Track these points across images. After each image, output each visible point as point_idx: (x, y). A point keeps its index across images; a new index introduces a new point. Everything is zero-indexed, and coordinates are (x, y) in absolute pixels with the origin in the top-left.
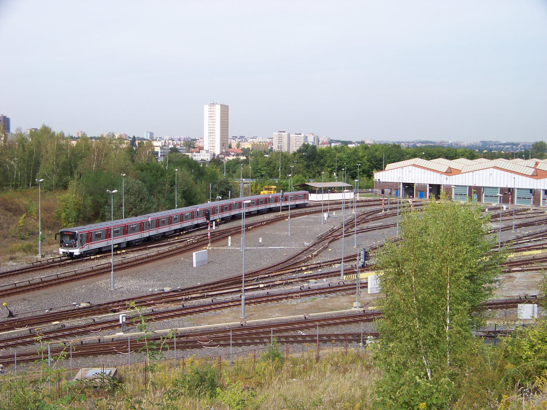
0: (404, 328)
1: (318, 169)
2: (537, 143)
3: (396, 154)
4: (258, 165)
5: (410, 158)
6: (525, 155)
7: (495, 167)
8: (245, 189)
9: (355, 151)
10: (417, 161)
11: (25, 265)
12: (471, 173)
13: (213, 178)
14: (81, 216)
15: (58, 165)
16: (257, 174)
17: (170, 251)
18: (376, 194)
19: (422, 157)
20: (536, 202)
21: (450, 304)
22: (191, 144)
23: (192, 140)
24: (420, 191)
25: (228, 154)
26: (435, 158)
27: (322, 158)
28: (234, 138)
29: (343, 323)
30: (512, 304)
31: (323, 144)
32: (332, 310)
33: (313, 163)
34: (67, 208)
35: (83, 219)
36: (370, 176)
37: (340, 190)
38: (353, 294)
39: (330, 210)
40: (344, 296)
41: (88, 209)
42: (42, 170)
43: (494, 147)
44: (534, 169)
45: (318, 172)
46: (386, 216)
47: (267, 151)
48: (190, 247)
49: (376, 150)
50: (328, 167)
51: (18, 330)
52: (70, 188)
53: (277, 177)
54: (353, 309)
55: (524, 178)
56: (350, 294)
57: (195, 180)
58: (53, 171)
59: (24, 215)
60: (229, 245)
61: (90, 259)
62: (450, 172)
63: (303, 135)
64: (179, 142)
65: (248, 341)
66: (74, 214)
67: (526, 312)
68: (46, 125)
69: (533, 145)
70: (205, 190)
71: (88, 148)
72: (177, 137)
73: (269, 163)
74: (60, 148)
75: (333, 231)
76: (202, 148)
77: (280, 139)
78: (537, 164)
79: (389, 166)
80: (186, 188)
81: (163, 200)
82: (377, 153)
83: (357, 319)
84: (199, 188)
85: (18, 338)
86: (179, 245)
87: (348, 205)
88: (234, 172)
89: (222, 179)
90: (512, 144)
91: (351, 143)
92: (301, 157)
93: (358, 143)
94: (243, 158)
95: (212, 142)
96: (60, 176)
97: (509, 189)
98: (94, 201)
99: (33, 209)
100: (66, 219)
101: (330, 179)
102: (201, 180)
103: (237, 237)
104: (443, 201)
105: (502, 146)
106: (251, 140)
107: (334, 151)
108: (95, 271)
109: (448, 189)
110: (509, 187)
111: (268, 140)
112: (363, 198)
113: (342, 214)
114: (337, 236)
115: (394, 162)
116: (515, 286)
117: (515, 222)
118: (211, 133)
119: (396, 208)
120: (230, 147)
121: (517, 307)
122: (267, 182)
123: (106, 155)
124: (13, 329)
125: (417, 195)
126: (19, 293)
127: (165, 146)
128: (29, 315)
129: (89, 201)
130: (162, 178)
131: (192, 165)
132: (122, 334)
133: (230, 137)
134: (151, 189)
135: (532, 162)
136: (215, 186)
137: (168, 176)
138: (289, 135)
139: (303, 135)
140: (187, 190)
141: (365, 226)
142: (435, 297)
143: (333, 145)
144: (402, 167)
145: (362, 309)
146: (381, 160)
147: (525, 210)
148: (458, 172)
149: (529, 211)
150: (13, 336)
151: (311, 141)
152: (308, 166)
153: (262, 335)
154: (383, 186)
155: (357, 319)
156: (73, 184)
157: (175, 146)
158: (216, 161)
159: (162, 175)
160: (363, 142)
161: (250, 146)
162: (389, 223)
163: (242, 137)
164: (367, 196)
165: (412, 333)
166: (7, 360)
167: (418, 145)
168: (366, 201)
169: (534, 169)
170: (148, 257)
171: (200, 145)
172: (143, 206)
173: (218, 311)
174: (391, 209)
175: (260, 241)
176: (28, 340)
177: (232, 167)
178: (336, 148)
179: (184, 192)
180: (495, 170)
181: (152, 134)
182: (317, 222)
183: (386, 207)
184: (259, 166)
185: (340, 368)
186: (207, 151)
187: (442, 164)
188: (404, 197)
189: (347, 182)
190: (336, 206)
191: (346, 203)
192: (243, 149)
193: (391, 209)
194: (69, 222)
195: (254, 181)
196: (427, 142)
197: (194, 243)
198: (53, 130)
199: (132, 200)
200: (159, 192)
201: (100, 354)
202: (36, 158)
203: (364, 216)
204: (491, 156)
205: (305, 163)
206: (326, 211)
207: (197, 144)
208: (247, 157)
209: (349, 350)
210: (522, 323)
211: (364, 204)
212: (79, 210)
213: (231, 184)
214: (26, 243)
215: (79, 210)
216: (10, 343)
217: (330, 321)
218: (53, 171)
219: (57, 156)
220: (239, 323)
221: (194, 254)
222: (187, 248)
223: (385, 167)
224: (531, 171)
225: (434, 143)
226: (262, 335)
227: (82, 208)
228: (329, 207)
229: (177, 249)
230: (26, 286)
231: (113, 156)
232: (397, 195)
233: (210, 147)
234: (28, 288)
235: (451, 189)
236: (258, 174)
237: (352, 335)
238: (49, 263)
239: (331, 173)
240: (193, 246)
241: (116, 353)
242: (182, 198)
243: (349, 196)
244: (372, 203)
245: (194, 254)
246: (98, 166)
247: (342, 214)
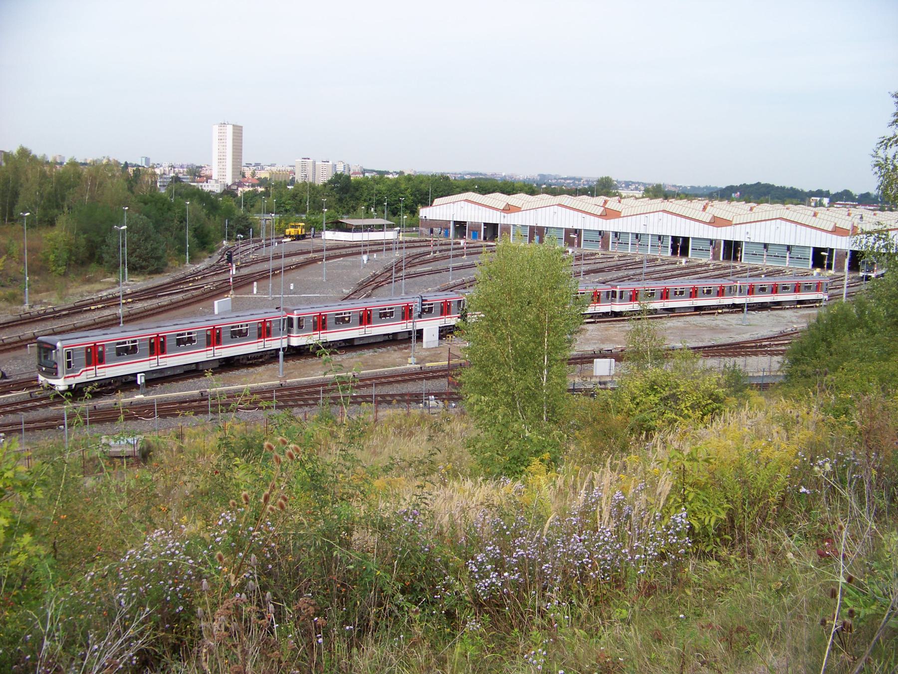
0: (500, 380)
1: (352, 203)
2: (602, 179)
3: (445, 186)
4: (281, 197)
5: (460, 193)
6: (590, 191)
7: (559, 205)
8: (268, 227)
9: (397, 183)
10: (471, 195)
11: (10, 318)
13: (229, 213)
14: (73, 258)
15: (42, 196)
16: (280, 208)
17: (184, 300)
18: (422, 234)
19: (474, 191)
20: (605, 246)
21: (549, 353)
22: (196, 172)
23: (197, 167)
24: (474, 231)
25: (240, 184)
26: (489, 193)
27: (357, 190)
28: (248, 165)
29: (398, 382)
30: (587, 359)
31: (355, 173)
32: (384, 367)
33: (347, 196)
34: (57, 249)
35: (76, 262)
36: (414, 212)
37: (380, 228)
38: (406, 349)
39: (370, 252)
40: (395, 351)
41: (82, 250)
42: (22, 201)
43: (554, 181)
45: (353, 207)
46: (435, 259)
47: (288, 181)
48: (208, 295)
49: (421, 182)
50: (365, 201)
51: (14, 394)
52: (58, 224)
53: (304, 212)
54: (408, 366)
55: (592, 218)
56: (402, 349)
57: (208, 215)
58: (36, 203)
59: (4, 257)
60: (255, 292)
61: (90, 310)
62: (508, 209)
63: (330, 163)
64: (181, 170)
65: (290, 403)
66: (65, 256)
67: (602, 367)
68: (25, 146)
69: (598, 181)
70: (219, 227)
71: (79, 176)
72: (179, 163)
73: (294, 196)
74: (43, 175)
75: (375, 276)
76: (209, 178)
77: (304, 166)
78: (606, 202)
79: (437, 201)
80: (198, 225)
81: (171, 239)
82: (423, 185)
83: (414, 377)
84: (212, 225)
85: (17, 404)
86: (195, 293)
87: (387, 246)
88: (252, 206)
89: (240, 215)
90: (574, 179)
91: (388, 173)
92: (332, 189)
93: (397, 173)
94: (261, 189)
95: (223, 170)
96: (45, 209)
97: (576, 230)
98: (89, 240)
99: (15, 249)
100: (56, 262)
101: (368, 215)
102: (214, 216)
103: (264, 282)
104: (499, 243)
105: (563, 181)
106: (269, 168)
107: (372, 183)
108: (97, 324)
109: (506, 228)
110: (575, 227)
111: (289, 169)
112: (407, 239)
113: (384, 257)
114: (381, 282)
115: (442, 196)
116: (588, 340)
117: (584, 268)
118: (221, 160)
119: (449, 250)
120: (244, 176)
121: (592, 362)
122: (293, 219)
123: (100, 184)
124: (9, 392)
125: (469, 235)
126: (8, 350)
127: (164, 174)
128: (25, 376)
129: (82, 239)
130: (170, 213)
131: (205, 198)
132: (142, 396)
133: (244, 164)
134: (157, 224)
135: (600, 199)
136: (231, 223)
137: (177, 211)
138: (314, 163)
139: (330, 163)
140: (199, 228)
141: (412, 270)
142: (532, 345)
143: (367, 174)
144: (454, 203)
145: (419, 366)
146: (427, 194)
147: (592, 255)
148: (518, 209)
149: (597, 256)
150: (11, 400)
151: (340, 169)
152: (340, 200)
153: (306, 397)
154: (432, 225)
155: (414, 377)
156: (62, 220)
157: (177, 174)
158: (229, 192)
159: (169, 209)
160: (401, 173)
161: (267, 176)
162: (439, 267)
163: (257, 165)
164: (411, 236)
165: (509, 386)
166: (8, 428)
167: (466, 177)
168: (410, 242)
170: (160, 307)
171: (208, 173)
172: (149, 247)
173: (251, 370)
174: (440, 251)
175: (292, 288)
176: (29, 405)
177: (250, 200)
178: (373, 178)
179: (195, 230)
181: (147, 160)
182: (356, 266)
183: (435, 248)
184: (283, 199)
185: (405, 431)
186: (217, 181)
187: (499, 199)
188: (455, 237)
189: (387, 219)
190: (376, 247)
191: (387, 243)
192: (259, 179)
193: (440, 251)
194: (59, 266)
195: (278, 217)
196: (477, 174)
197: (212, 291)
198: (34, 152)
199: (135, 239)
200: (167, 229)
201: (106, 421)
202: (13, 187)
203: (410, 259)
204: (553, 192)
205: (337, 196)
206: (365, 253)
207: (204, 172)
208: (266, 188)
209: (411, 411)
210: (598, 380)
211: (416, 244)
212: (70, 251)
213: (250, 221)
214: (9, 291)
215: (70, 251)
216: (8, 409)
217: (383, 380)
218: (36, 203)
219: (41, 185)
220: (278, 382)
221: (216, 302)
222: (205, 296)
223: (432, 202)
224: (599, 211)
226: (306, 397)
227: (73, 248)
228: (368, 249)
229: (194, 297)
230: (16, 343)
231: (110, 185)
232: (447, 235)
233: (219, 177)
234: (19, 344)
235: (509, 228)
236: (282, 209)
237: (411, 395)
238: (40, 315)
239: (368, 208)
240: (211, 294)
241: (136, 419)
242: (194, 237)
243: (390, 235)
244: (418, 244)
245: (216, 302)
246: (91, 197)
247: (384, 257)
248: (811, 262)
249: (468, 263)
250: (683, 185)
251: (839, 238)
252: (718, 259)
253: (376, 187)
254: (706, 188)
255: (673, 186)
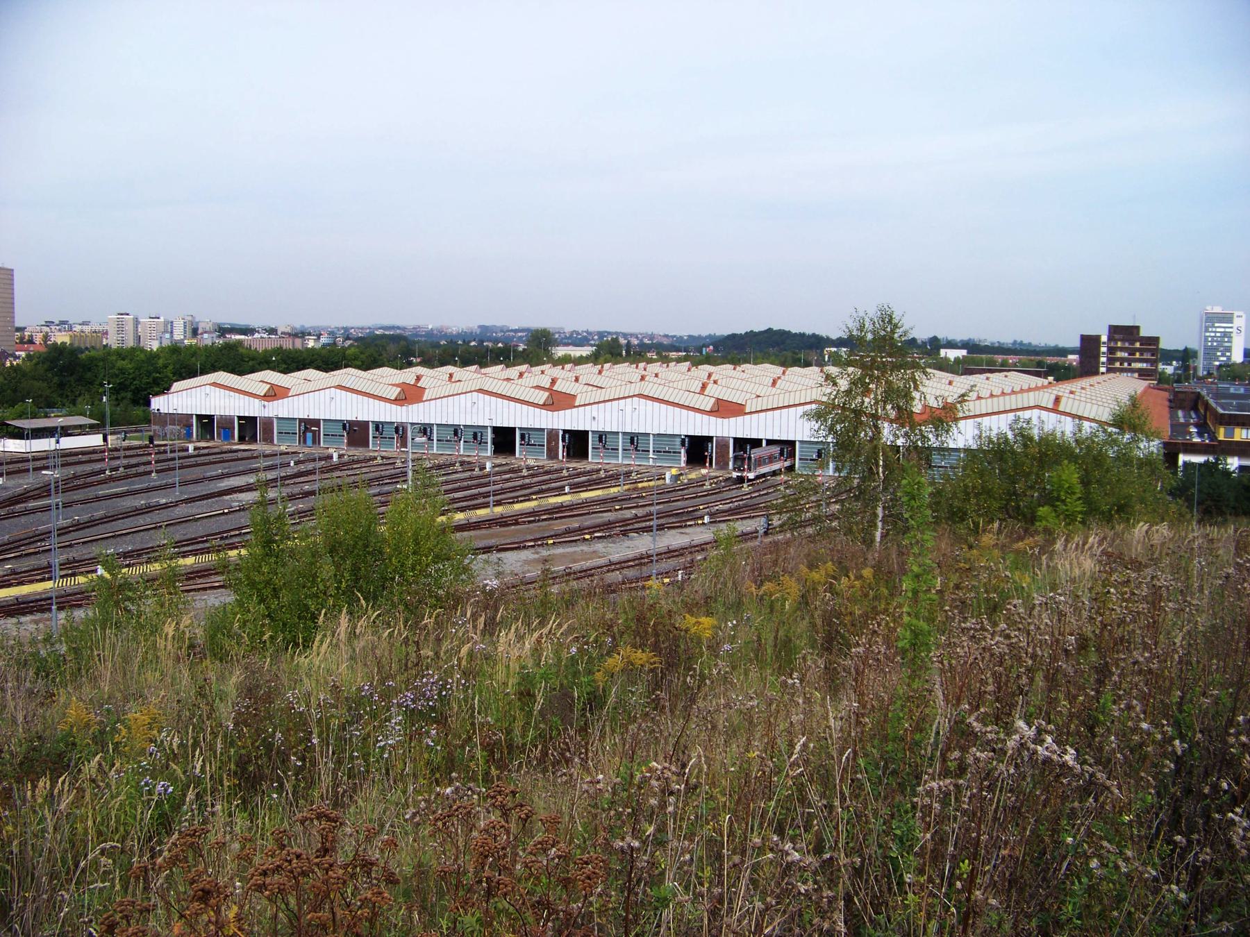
7: (340, 387)
10: (222, 377)
12: (601, 405)
33: (72, 379)
44: (547, 394)
63: (162, 319)
77: (120, 327)
79: (177, 386)
109: (268, 423)
138: (136, 322)
139: (162, 319)
152: (61, 385)
169: (547, 394)
180: (481, 395)
187: (387, 378)
193: (125, 467)
205: (56, 379)
225: (404, 329)
235: (272, 423)
248: (683, 458)
249: (157, 483)
250: (678, 334)
251: (720, 420)
252: (556, 456)
253: (120, 363)
254: (710, 336)
255: (666, 336)
